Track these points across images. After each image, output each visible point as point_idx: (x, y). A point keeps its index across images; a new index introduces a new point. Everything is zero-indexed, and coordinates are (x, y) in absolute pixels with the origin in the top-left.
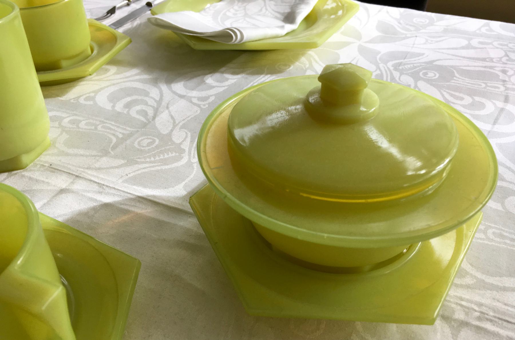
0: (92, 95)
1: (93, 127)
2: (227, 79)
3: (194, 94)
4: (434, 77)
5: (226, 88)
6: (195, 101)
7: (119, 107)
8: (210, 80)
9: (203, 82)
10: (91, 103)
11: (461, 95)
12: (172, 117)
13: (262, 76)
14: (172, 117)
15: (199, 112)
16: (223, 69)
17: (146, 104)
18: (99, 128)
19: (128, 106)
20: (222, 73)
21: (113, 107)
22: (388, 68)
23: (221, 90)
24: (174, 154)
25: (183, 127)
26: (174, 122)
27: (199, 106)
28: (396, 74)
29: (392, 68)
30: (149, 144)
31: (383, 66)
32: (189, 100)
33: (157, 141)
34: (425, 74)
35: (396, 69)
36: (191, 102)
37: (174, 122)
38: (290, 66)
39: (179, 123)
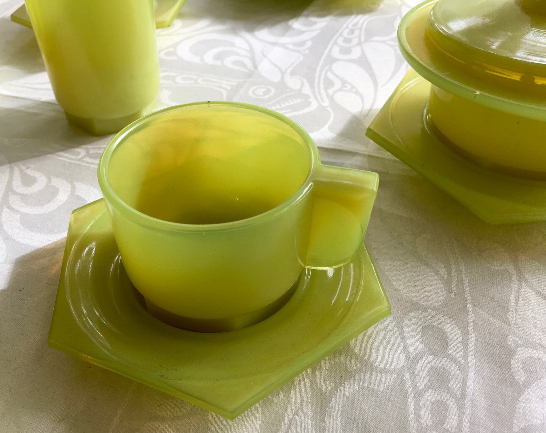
0: (171, 50)
1: (193, 82)
2: (315, 23)
3: (285, 40)
4: (255, 90)
5: (318, 31)
6: (291, 47)
7: (209, 58)
8: (297, 24)
9: (290, 27)
10: (175, 58)
11: (236, 68)
12: (276, 66)
13: (353, 17)
14: (276, 66)
15: (302, 58)
16: (305, 12)
17: (237, 54)
18: (200, 81)
19: (218, 57)
20: (307, 16)
21: (202, 59)
22: (316, 98)
23: (315, 33)
24: (299, 100)
25: (293, 73)
26: (280, 70)
27: (298, 52)
28: (307, 90)
29: (312, 99)
30: (265, 93)
31: (323, 102)
32: (284, 46)
33: (273, 91)
34: (268, 92)
35: (307, 97)
36: (287, 48)
37: (280, 70)
38: (379, 5)
39: (286, 70)
